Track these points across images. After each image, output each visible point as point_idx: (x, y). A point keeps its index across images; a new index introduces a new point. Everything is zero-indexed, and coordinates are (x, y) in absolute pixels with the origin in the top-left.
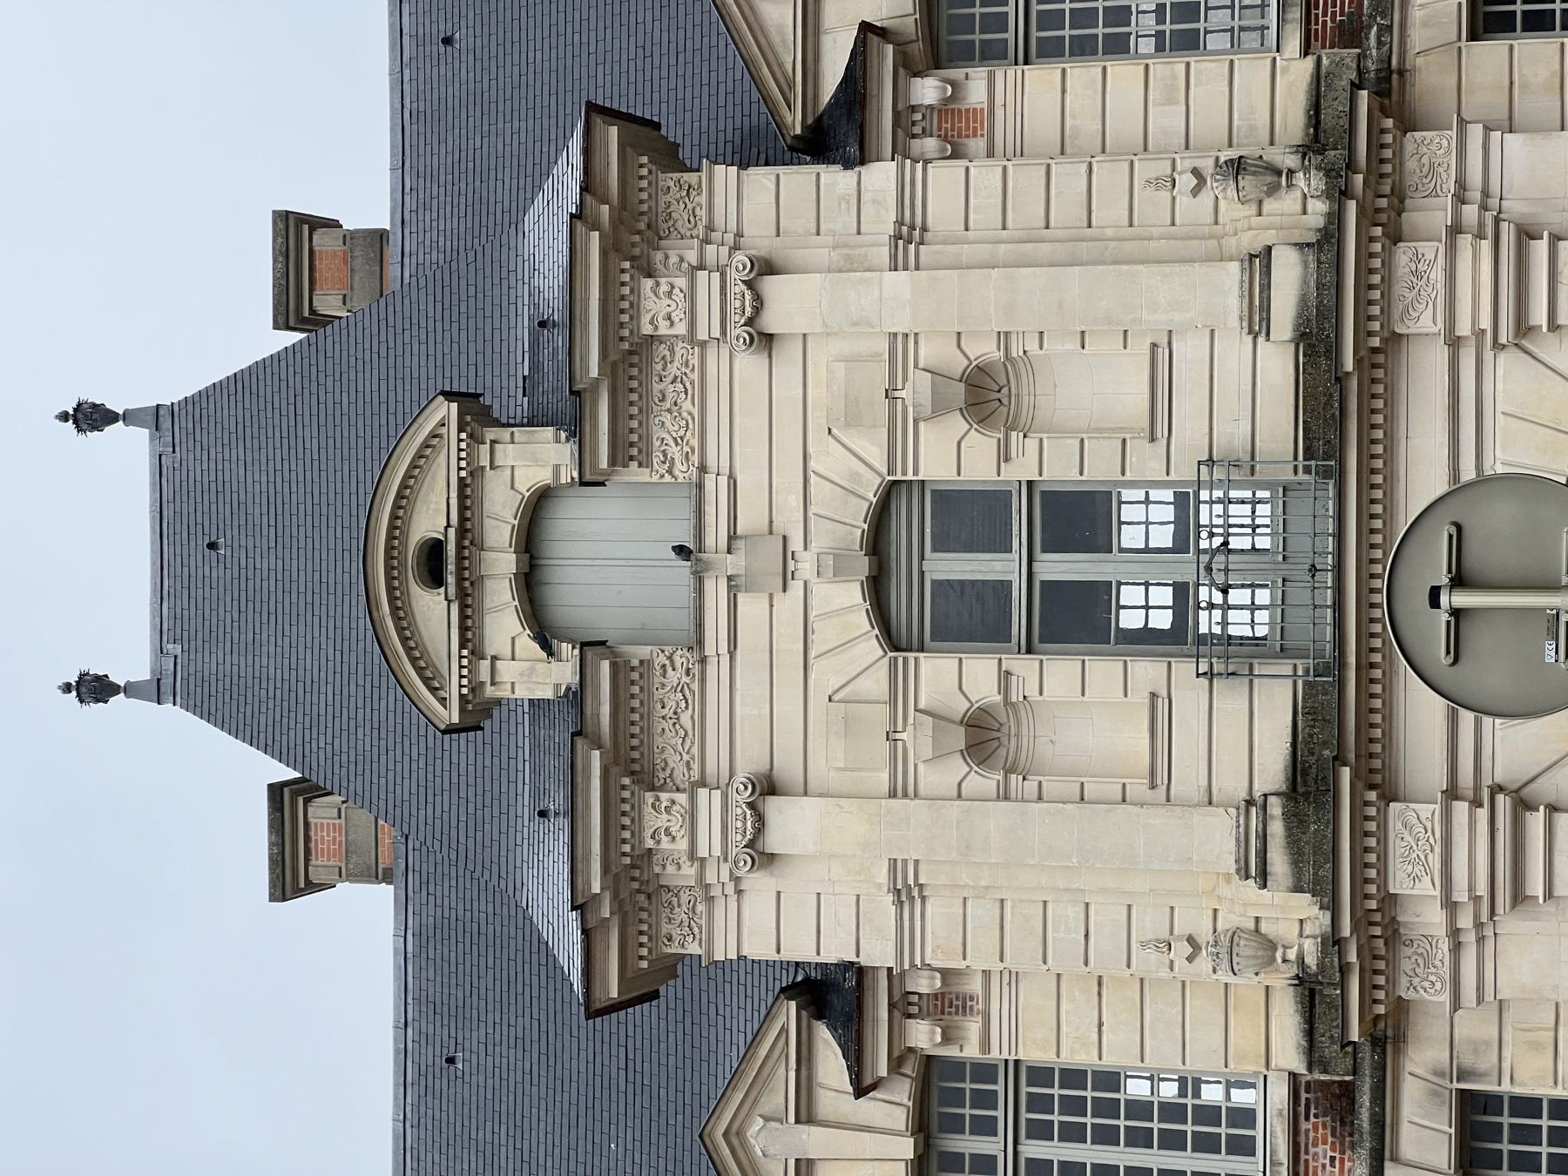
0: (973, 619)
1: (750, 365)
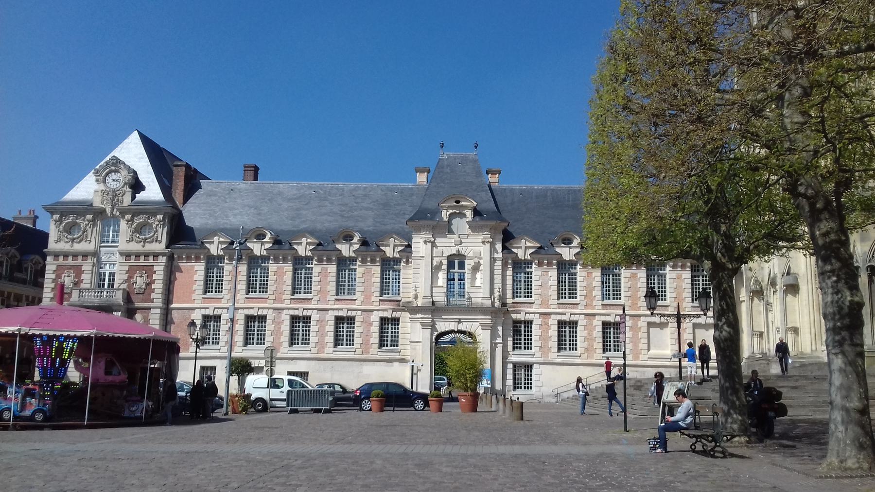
0: (451, 265)
1: (480, 240)
